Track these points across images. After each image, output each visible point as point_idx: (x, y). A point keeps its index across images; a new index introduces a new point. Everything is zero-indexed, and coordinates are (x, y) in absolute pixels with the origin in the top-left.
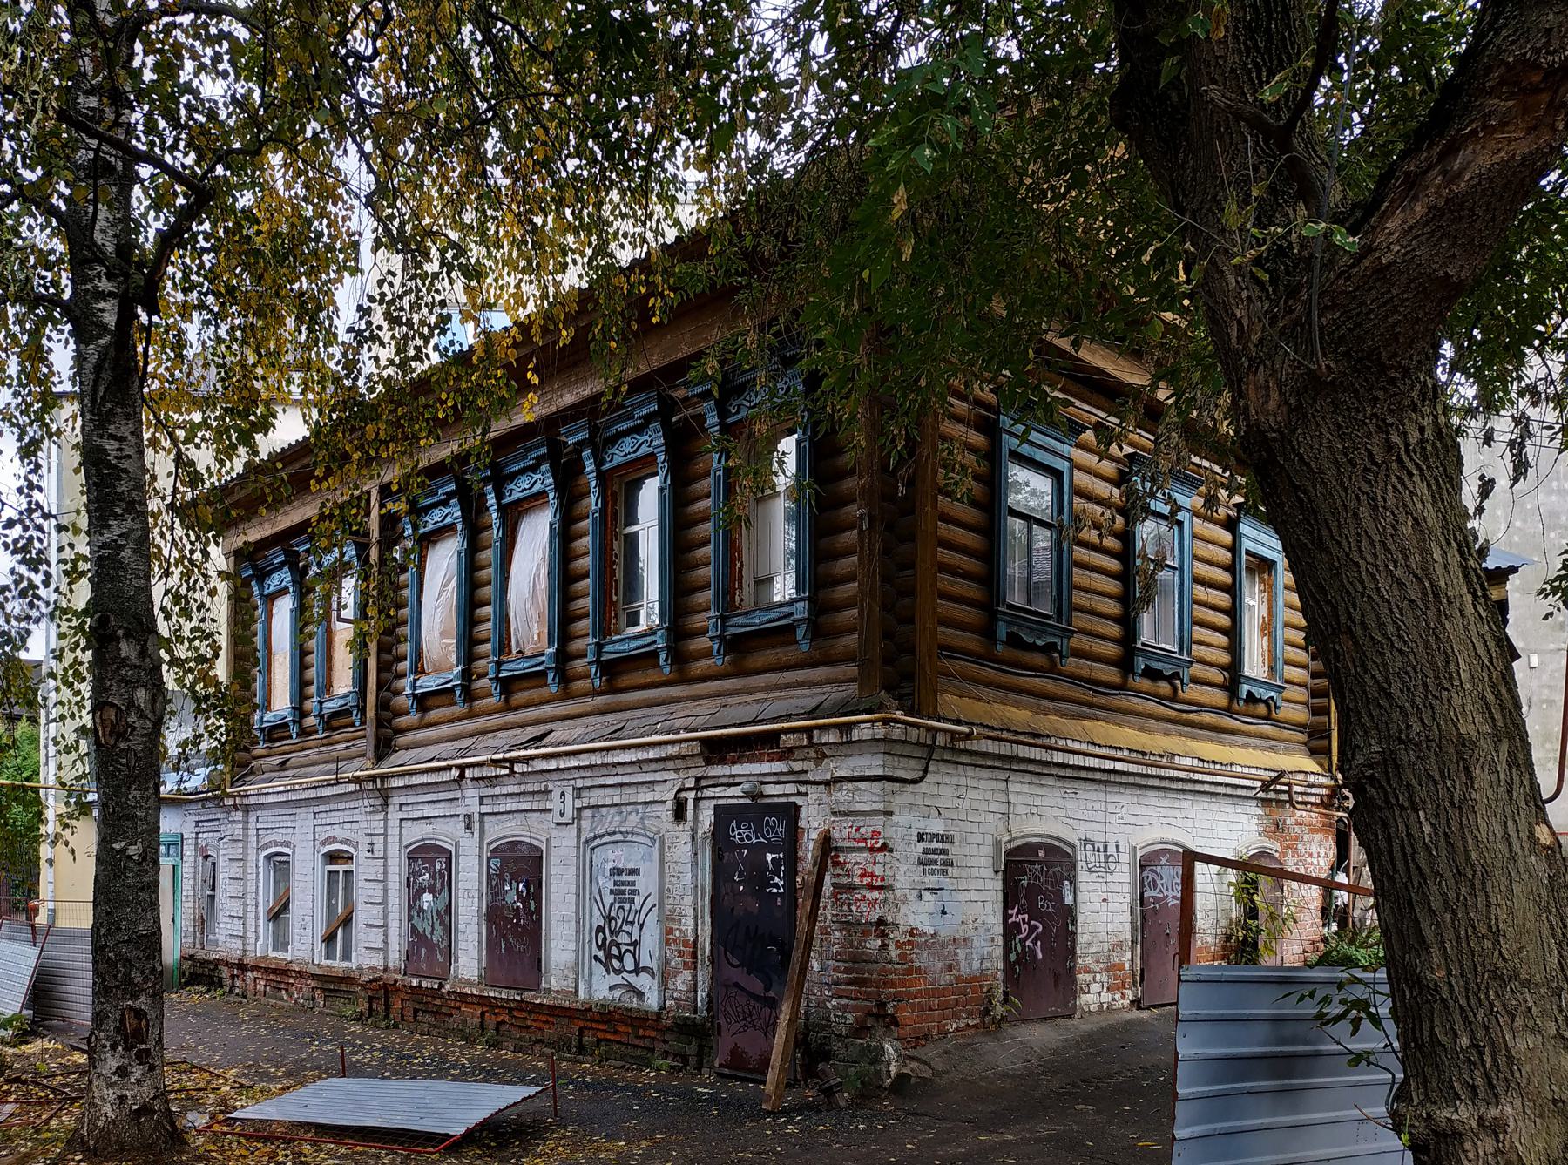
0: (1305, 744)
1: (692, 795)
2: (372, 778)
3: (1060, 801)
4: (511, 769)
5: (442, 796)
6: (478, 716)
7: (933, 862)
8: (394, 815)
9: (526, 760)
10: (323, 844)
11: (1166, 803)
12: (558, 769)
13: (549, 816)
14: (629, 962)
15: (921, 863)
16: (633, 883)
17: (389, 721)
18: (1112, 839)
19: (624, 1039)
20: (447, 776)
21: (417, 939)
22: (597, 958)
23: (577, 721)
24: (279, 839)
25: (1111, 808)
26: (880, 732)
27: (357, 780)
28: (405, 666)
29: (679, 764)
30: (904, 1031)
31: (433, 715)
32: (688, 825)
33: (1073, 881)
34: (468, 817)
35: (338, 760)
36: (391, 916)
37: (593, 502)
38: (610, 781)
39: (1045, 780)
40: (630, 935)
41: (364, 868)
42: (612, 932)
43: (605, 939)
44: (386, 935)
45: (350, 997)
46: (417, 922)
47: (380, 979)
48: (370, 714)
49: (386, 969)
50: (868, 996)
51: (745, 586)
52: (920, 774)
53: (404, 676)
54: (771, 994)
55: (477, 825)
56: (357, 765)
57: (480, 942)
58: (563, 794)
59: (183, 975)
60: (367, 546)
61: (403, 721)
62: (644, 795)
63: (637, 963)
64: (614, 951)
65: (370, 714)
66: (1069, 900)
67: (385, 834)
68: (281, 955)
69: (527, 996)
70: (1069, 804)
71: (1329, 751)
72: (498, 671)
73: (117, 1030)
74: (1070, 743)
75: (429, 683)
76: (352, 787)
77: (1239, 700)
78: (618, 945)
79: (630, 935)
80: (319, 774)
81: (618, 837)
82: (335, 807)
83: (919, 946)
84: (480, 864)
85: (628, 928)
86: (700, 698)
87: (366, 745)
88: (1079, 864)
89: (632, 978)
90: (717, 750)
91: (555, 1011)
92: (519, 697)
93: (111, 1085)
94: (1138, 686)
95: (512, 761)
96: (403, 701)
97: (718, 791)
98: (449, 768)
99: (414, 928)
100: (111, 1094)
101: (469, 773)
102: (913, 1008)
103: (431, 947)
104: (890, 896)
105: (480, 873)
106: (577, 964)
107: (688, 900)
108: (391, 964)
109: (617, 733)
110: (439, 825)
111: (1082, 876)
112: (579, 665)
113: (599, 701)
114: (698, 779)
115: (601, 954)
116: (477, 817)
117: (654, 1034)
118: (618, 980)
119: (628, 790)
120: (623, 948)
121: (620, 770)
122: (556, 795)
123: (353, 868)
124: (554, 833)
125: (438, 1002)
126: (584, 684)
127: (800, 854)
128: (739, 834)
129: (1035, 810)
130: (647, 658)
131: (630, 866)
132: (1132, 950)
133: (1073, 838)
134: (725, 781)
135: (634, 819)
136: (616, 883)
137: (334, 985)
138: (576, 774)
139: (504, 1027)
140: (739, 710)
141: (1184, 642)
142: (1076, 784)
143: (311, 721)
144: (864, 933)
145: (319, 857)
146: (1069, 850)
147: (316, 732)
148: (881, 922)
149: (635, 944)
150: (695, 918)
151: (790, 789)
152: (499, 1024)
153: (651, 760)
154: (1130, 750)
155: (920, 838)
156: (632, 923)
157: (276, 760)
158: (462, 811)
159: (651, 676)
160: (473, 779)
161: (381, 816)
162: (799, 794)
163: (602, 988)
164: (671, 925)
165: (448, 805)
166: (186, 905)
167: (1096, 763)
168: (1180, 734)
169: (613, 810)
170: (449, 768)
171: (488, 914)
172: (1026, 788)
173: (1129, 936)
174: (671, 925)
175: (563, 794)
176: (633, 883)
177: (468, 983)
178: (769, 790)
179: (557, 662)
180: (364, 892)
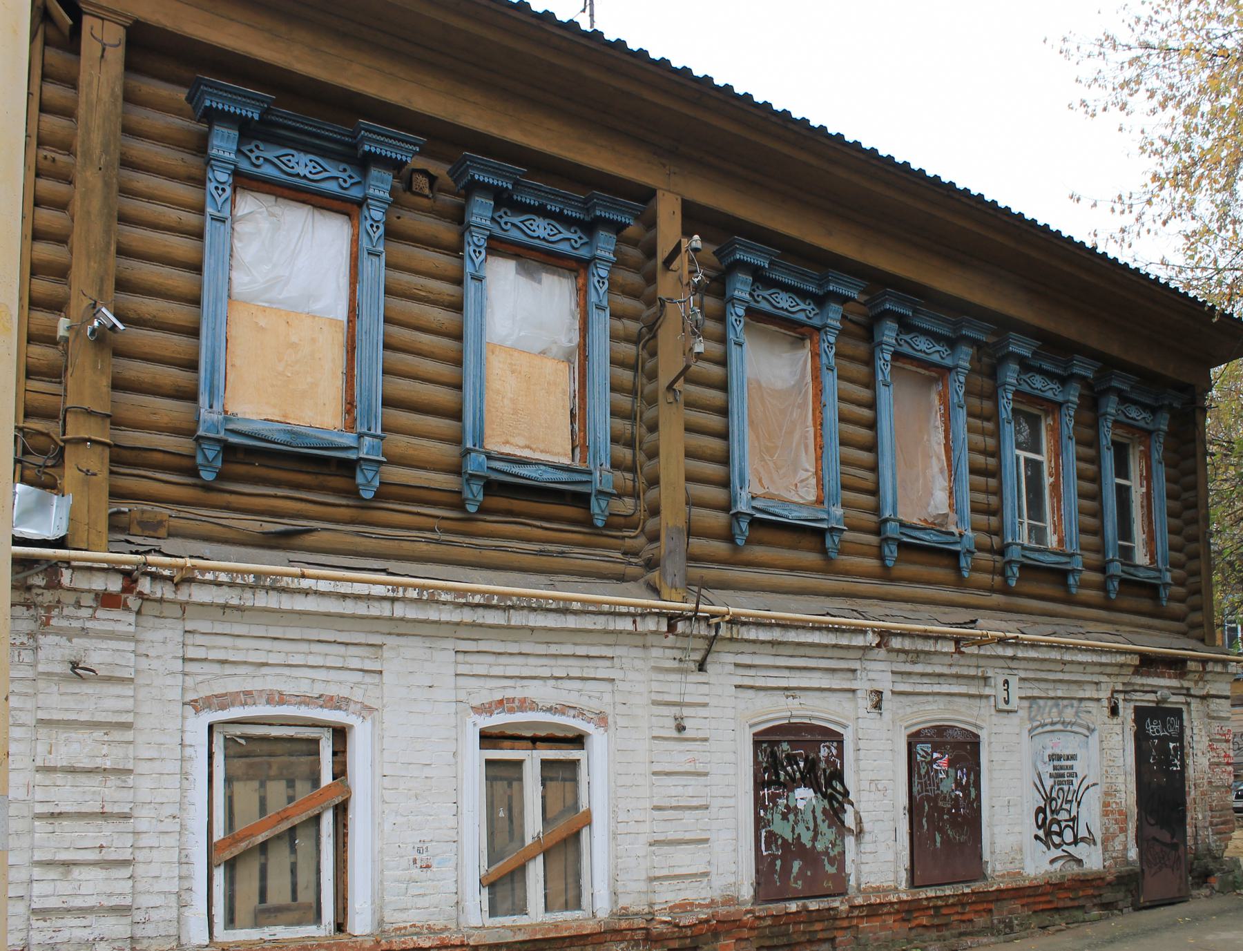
6: (837, 573)
14: (1068, 836)
16: (1071, 767)
20: (859, 641)
22: (1037, 837)
42: (1052, 812)
43: (1045, 819)
58: (1006, 682)
62: (1089, 692)
63: (1075, 836)
64: (1055, 828)
69: (978, 886)
78: (1059, 822)
79: (1069, 812)
81: (1059, 727)
82: (542, 649)
90: (1148, 663)
91: (1001, 895)
107: (1121, 779)
118: (1059, 853)
120: (1063, 824)
128: (1153, 728)
136: (1055, 768)
149: (1074, 819)
151: (1182, 699)
156: (1071, 801)
163: (1038, 864)
165: (828, 676)
169: (1050, 703)
170: (862, 631)
175: (1006, 682)
176: (1071, 767)
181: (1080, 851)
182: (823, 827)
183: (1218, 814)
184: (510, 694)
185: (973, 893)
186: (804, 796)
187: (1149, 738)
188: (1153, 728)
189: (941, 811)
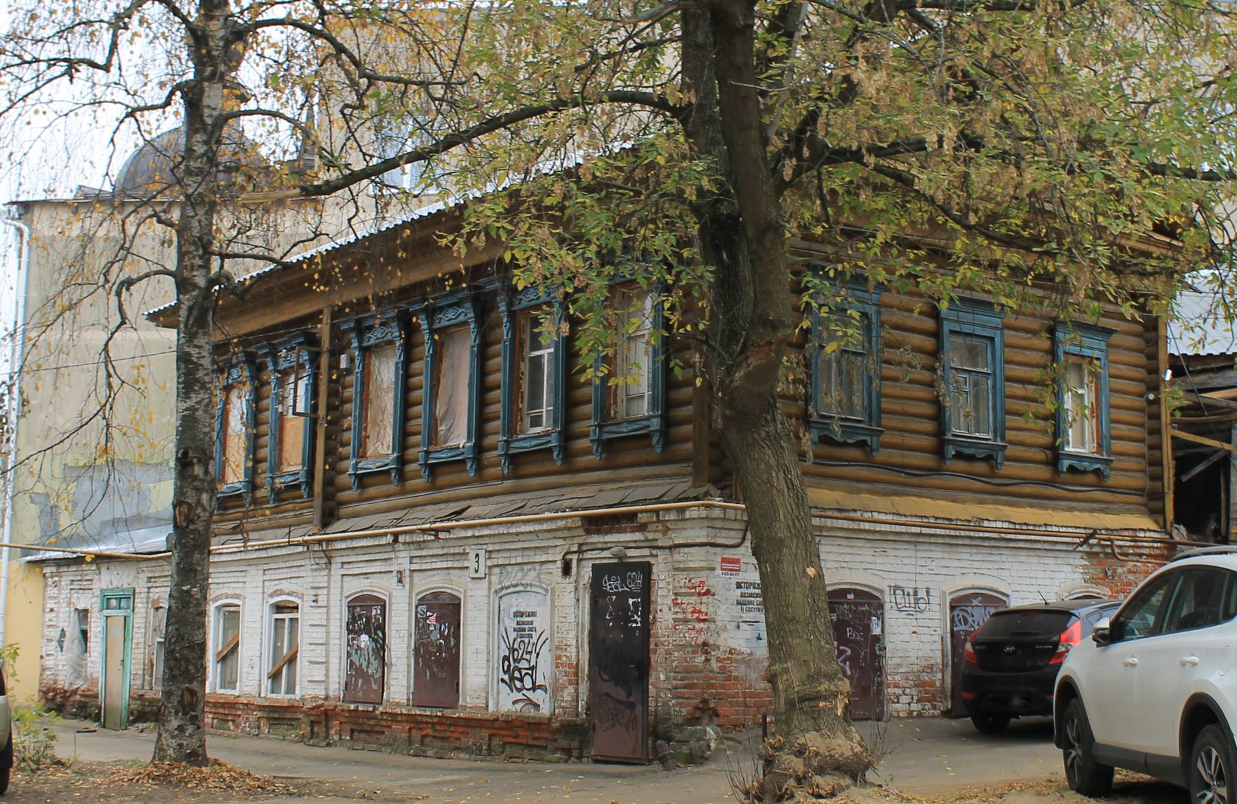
0: (1145, 505)
1: (575, 557)
2: (320, 542)
3: (871, 559)
4: (436, 536)
5: (378, 556)
7: (751, 603)
8: (336, 571)
9: (448, 530)
10: (271, 596)
11: (979, 557)
12: (474, 537)
13: (465, 572)
14: (528, 682)
15: (739, 603)
16: (532, 623)
17: (333, 496)
18: (922, 586)
19: (524, 741)
20: (383, 541)
21: (355, 672)
22: (503, 680)
23: (490, 499)
24: (230, 592)
25: (922, 562)
26: (703, 513)
27: (305, 543)
28: (349, 450)
29: (566, 533)
30: (722, 721)
31: (372, 491)
32: (573, 579)
33: (881, 618)
34: (400, 572)
35: (290, 526)
36: (332, 654)
37: (505, 331)
38: (513, 546)
39: (854, 543)
40: (529, 661)
41: (307, 615)
42: (515, 660)
43: (509, 666)
44: (327, 670)
45: (292, 723)
46: (355, 658)
47: (322, 705)
48: (318, 487)
49: (326, 698)
50: (697, 695)
51: (619, 402)
52: (739, 541)
53: (348, 458)
54: (632, 699)
55: (407, 580)
56: (305, 530)
57: (409, 672)
58: (477, 555)
59: (132, 713)
60: (318, 354)
61: (345, 495)
63: (534, 683)
64: (517, 674)
65: (318, 487)
66: (877, 631)
67: (328, 587)
68: (229, 692)
69: (448, 712)
70: (878, 560)
71: (1162, 512)
72: (427, 458)
73: (179, 702)
74: (875, 515)
75: (369, 465)
76: (300, 549)
77: (1061, 475)
78: (520, 670)
79: (529, 661)
80: (272, 537)
82: (283, 565)
83: (736, 661)
84: (410, 611)
85: (527, 657)
86: (585, 484)
87: (314, 514)
88: (887, 606)
89: (530, 694)
90: (595, 524)
91: (471, 724)
92: (443, 479)
93: (173, 737)
94: (953, 467)
95: (437, 530)
96: (344, 479)
97: (595, 554)
98: (385, 534)
99: (352, 663)
100: (174, 742)
101: (401, 539)
102: (732, 704)
103: (367, 678)
104: (712, 626)
105: (410, 618)
106: (487, 685)
107: (572, 634)
108: (331, 694)
109: (519, 510)
110: (375, 579)
111: (890, 613)
112: (491, 455)
113: (508, 484)
114: (580, 545)
115: (506, 677)
116: (407, 573)
117: (546, 735)
118: (519, 696)
119: (527, 553)
120: (524, 672)
121: (522, 537)
122: (472, 556)
123: (298, 615)
124: (470, 585)
125: (372, 722)
126: (496, 471)
127: (653, 598)
128: (610, 585)
129: (844, 565)
130: (543, 453)
131: (529, 609)
132: (943, 671)
133: (884, 585)
134: (599, 546)
135: (533, 574)
137: (279, 716)
138: (487, 540)
139: (428, 740)
140: (605, 496)
141: (1000, 431)
142: (885, 545)
143: (261, 493)
144: (694, 652)
145: (267, 608)
146: (878, 594)
147: (268, 502)
148: (705, 644)
149: (532, 668)
150: (577, 647)
151: (646, 552)
152: (424, 737)
153: (545, 531)
154: (936, 518)
155: (739, 585)
157: (231, 525)
158: (395, 568)
159: (548, 467)
160: (404, 543)
161: (325, 572)
162: (652, 555)
163: (505, 703)
164: (559, 652)
166: (136, 651)
167: (903, 529)
168: (996, 503)
169: (516, 568)
170: (385, 534)
171: (417, 650)
172: (836, 549)
173: (939, 661)
174: (559, 652)
175: (477, 555)
176: (532, 623)
177: (398, 704)
178: (630, 553)
179: (474, 453)
180: (306, 635)
181: (537, 696)
182: (372, 659)
183: (679, 676)
184: (278, 587)
185: (443, 716)
186: (364, 638)
187: (606, 594)
188: (610, 585)
189: (431, 654)
